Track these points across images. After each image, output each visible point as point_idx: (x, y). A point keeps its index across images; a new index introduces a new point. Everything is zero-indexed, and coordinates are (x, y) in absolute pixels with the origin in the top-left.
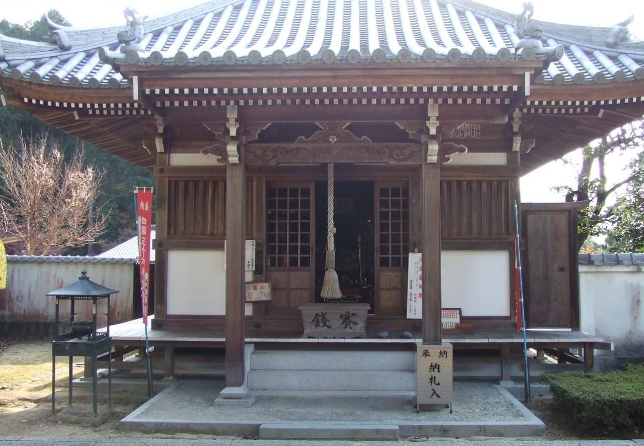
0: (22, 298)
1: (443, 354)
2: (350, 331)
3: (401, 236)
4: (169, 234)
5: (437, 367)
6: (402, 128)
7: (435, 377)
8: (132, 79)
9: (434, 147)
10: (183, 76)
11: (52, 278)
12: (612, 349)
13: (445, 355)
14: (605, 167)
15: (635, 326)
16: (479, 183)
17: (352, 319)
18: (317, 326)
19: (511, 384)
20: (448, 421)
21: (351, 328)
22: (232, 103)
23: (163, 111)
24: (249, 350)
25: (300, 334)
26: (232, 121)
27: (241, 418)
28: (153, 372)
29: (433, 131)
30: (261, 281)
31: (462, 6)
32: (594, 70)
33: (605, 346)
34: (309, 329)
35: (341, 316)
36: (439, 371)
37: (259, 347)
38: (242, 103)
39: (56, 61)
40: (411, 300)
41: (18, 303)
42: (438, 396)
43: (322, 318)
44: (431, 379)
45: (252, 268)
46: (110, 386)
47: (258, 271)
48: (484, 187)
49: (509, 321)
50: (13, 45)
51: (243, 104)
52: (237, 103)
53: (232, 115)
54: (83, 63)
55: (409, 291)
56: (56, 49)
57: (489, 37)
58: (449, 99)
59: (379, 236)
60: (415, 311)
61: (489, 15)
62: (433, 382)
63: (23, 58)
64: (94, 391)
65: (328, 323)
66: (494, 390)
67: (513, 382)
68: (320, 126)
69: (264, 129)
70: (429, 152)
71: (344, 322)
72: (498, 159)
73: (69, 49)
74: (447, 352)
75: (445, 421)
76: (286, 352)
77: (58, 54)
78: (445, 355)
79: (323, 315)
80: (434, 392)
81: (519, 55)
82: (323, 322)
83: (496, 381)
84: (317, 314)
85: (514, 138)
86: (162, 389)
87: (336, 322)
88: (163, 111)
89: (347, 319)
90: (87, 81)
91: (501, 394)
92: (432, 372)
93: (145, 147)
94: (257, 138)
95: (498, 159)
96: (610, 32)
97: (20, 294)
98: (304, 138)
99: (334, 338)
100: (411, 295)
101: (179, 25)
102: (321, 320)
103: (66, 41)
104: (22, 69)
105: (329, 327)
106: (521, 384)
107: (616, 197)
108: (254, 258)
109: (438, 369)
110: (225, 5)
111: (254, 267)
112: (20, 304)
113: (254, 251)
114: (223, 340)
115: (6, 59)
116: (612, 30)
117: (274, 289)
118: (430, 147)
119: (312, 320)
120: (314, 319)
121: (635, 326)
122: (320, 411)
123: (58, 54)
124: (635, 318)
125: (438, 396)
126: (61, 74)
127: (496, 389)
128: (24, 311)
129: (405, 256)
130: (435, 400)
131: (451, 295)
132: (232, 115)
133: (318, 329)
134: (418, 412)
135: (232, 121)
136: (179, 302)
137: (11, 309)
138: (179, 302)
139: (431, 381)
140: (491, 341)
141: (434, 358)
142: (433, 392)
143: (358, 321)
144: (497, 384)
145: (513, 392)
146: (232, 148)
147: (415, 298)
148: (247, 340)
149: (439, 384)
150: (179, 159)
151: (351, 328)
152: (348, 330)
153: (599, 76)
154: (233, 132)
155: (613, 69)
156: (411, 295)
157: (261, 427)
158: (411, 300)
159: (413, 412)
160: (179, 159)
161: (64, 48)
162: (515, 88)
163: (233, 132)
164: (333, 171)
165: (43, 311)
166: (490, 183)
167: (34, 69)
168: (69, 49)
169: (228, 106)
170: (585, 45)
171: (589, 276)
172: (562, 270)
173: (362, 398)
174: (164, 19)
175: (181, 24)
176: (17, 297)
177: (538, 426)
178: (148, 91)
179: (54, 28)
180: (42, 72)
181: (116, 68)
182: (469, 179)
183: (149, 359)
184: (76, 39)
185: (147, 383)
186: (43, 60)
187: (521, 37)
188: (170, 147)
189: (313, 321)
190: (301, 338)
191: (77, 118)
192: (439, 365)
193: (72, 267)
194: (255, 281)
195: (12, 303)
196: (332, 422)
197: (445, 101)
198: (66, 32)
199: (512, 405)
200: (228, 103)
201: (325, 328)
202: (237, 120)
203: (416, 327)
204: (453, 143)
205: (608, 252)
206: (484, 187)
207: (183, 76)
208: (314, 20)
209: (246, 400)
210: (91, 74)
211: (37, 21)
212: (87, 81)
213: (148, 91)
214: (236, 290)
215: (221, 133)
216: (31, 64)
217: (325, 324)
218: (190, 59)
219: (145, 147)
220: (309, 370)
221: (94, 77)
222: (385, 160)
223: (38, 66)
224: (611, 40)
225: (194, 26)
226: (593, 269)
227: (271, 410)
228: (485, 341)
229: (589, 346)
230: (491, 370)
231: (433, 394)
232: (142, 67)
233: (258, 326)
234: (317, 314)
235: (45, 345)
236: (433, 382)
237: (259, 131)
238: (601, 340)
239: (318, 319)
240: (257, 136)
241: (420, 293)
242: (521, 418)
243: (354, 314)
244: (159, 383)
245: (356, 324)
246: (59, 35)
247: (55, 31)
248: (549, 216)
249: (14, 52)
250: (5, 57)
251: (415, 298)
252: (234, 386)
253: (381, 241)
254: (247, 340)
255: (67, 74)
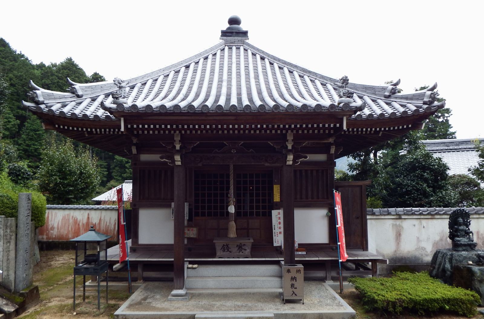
0: (54, 228)
1: (298, 271)
2: (242, 254)
3: (254, 181)
4: (140, 199)
6: (272, 145)
8: (121, 119)
9: (290, 157)
10: (150, 118)
11: (71, 217)
12: (388, 263)
13: (299, 272)
15: (398, 248)
16: (312, 171)
17: (243, 247)
18: (224, 251)
19: (331, 282)
20: (301, 310)
21: (243, 252)
22: (178, 132)
23: (137, 136)
24: (186, 265)
25: (214, 256)
26: (177, 142)
27: (184, 310)
29: (290, 147)
30: (192, 227)
31: (302, 72)
32: (379, 112)
33: (383, 261)
34: (219, 253)
35: (237, 246)
36: (296, 281)
37: (190, 263)
38: (183, 132)
39: (73, 103)
40: (275, 236)
41: (51, 231)
42: (296, 295)
43: (226, 247)
44: (292, 285)
45: (187, 218)
46: (107, 287)
47: (190, 219)
48: (315, 173)
49: (329, 246)
50: (49, 95)
51: (184, 133)
52: (180, 132)
53: (177, 138)
54: (89, 105)
55: (274, 231)
56: (74, 97)
57: (316, 86)
58: (299, 131)
60: (278, 242)
61: (317, 78)
62: (293, 287)
63: (54, 102)
64: (99, 293)
65: (230, 250)
66: (323, 287)
67: (333, 281)
68: (227, 144)
69: (195, 145)
70: (288, 159)
71: (239, 249)
72: (322, 157)
73: (82, 96)
75: (299, 310)
76: (207, 266)
77: (76, 99)
78: (299, 272)
79: (227, 245)
80: (294, 292)
81: (340, 107)
82: (227, 249)
83: (323, 280)
84: (224, 245)
85: (332, 147)
86: (137, 288)
87: (234, 249)
88: (137, 136)
89: (240, 247)
90: (93, 116)
91: (327, 290)
93: (126, 151)
94: (191, 150)
95: (322, 157)
96: (386, 89)
97: (53, 226)
98: (217, 150)
99: (233, 258)
100: (275, 233)
101: (145, 82)
102: (226, 248)
103: (80, 93)
104: (54, 108)
105: (231, 252)
106: (337, 282)
107: (252, 40)
108: (188, 213)
109: (296, 280)
110: (170, 71)
111: (188, 217)
112: (52, 232)
113: (188, 209)
114: (173, 260)
115: (45, 102)
116: (388, 88)
117: (199, 230)
118: (288, 157)
119: (221, 248)
120: (222, 247)
121: (398, 248)
122: (229, 303)
123: (76, 99)
124: (398, 243)
125: (296, 295)
126: (77, 112)
127: (324, 286)
128: (55, 235)
130: (294, 298)
131: (301, 237)
132: (177, 138)
133: (225, 253)
134: (284, 304)
135: (177, 142)
136: (146, 236)
137: (47, 235)
138: (146, 236)
139: (292, 286)
140: (320, 259)
141: (293, 274)
143: (246, 248)
144: (323, 282)
145: (332, 287)
146: (177, 158)
147: (277, 234)
148: (186, 259)
149: (296, 288)
150: (145, 157)
151: (243, 252)
152: (241, 253)
153: (382, 115)
154: (178, 147)
155: (390, 111)
156: (275, 233)
157: (196, 316)
158: (275, 236)
159: (282, 303)
160: (145, 157)
161: (78, 96)
162: (338, 125)
163: (178, 147)
164: (232, 167)
165: (66, 236)
166: (317, 171)
167: (62, 108)
168: (82, 96)
169: (175, 134)
170: (372, 96)
171: (373, 221)
172: (358, 218)
173: (250, 293)
174: (136, 79)
175: (146, 82)
176: (51, 228)
177: (352, 313)
178: (129, 126)
179: (73, 85)
180: (65, 110)
181: (111, 113)
182: (306, 168)
183: (129, 272)
184: (86, 91)
185: (127, 284)
186: (67, 103)
187: (341, 97)
188: (140, 151)
189: (221, 249)
190: (215, 258)
191: (87, 135)
192: (296, 278)
193: (82, 211)
194: (189, 226)
195: (48, 231)
196: (236, 312)
197: (297, 131)
198: (80, 87)
199: (335, 297)
200: (175, 132)
201: (228, 252)
202: (180, 141)
203: (278, 251)
204: (301, 154)
206: (315, 173)
207: (150, 118)
208: (220, 81)
209: (186, 297)
210: (95, 112)
211: (56, 64)
212: (93, 116)
213: (129, 126)
214: (179, 232)
215: (170, 147)
216: (59, 105)
217: (228, 251)
218: (154, 109)
219: (126, 151)
220: (220, 277)
221: (97, 114)
222: (263, 163)
223: (64, 106)
224: (387, 94)
225: (153, 83)
226: (375, 217)
227: (200, 303)
228: (317, 259)
229: (374, 261)
230: (320, 274)
231: (293, 294)
232: (126, 113)
233: (190, 250)
234: (224, 245)
237: (192, 147)
238: (381, 258)
239: (224, 248)
240: (191, 149)
242: (342, 308)
243: (244, 245)
244: (135, 285)
245: (246, 250)
246: (75, 89)
247: (73, 86)
248: (350, 189)
249: (49, 99)
250: (44, 101)
251: (277, 234)
252: (179, 289)
254: (186, 259)
255: (81, 112)
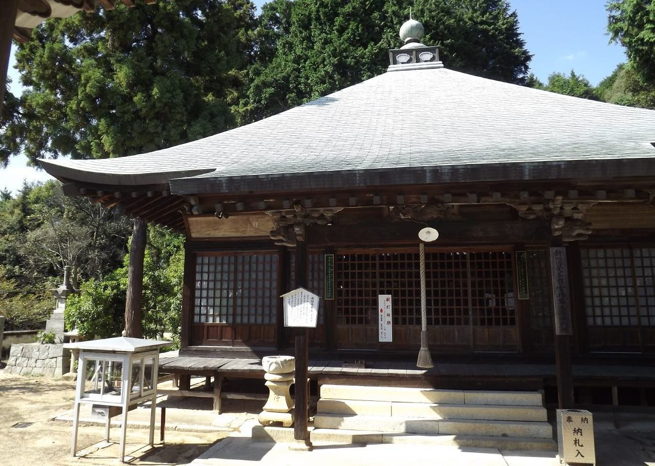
5: (580, 431)
7: (578, 440)
14: (301, 452)
28: (241, 209)
36: (581, 435)
44: (575, 441)
59: (404, 253)
62: (577, 444)
74: (581, 430)
80: (579, 452)
92: (576, 435)
129: (385, 291)
139: (575, 443)
142: (577, 452)
149: (582, 446)
205: (631, 94)
235: (297, 161)
236: (577, 444)
241: (4, 372)
253: (467, 300)
